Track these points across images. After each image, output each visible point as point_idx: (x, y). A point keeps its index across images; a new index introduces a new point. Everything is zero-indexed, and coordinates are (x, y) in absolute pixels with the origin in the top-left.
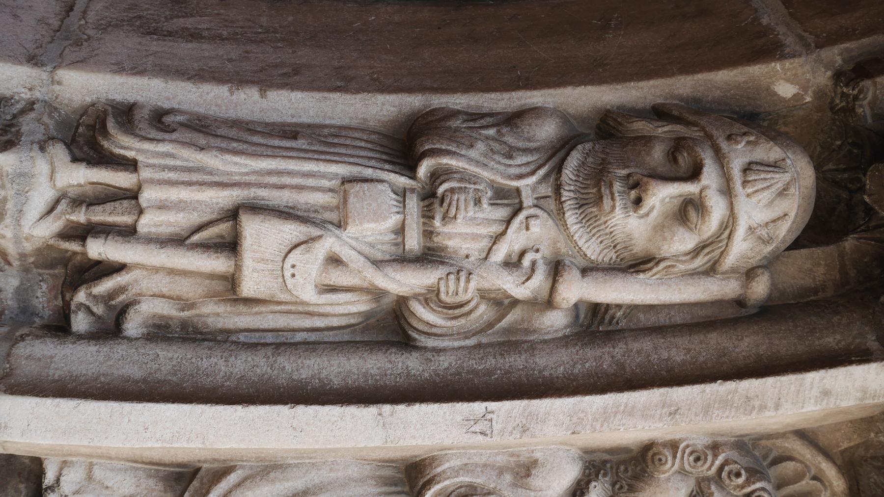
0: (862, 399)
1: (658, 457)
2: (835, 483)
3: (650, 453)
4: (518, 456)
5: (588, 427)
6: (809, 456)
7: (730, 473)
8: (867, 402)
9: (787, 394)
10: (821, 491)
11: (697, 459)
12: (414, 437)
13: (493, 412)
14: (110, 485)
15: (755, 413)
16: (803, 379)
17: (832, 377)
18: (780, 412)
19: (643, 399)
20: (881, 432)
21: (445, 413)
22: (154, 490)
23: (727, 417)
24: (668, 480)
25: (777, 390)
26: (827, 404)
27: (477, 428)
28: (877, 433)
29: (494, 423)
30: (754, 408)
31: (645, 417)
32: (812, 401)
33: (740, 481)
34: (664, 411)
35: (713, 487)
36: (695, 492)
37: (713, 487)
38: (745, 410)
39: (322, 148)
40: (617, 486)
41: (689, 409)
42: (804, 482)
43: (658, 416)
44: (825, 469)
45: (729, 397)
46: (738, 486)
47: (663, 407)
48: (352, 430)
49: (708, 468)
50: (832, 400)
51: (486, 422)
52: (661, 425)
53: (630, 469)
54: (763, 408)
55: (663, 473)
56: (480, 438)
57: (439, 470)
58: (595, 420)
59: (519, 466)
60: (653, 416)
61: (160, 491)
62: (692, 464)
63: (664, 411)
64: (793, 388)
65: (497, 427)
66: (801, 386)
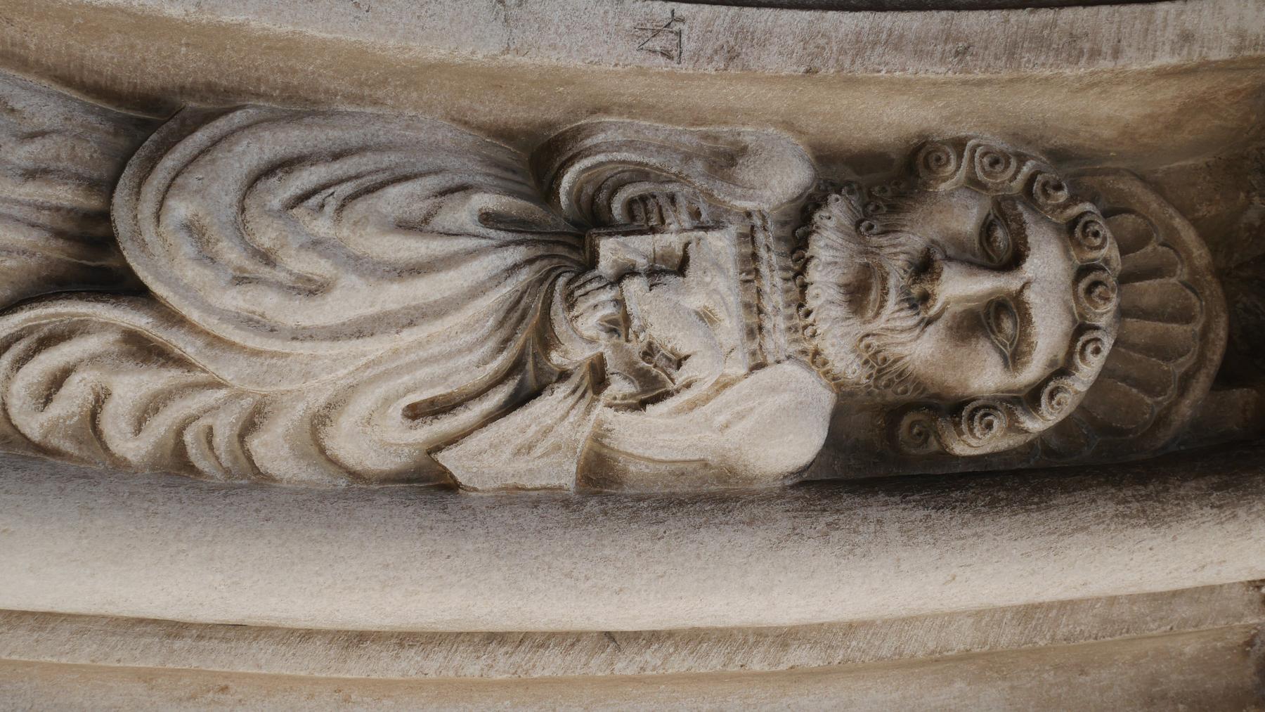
0: (1239, 49)
1: (934, 156)
2: (1196, 253)
3: (922, 155)
4: (716, 139)
5: (831, 62)
6: (1154, 206)
7: (1045, 185)
8: (1247, 53)
9: (1130, 34)
10: (1176, 264)
11: (994, 162)
12: (554, 47)
13: (682, 20)
14: (18, 106)
15: (1083, 61)
16: (1153, 12)
17: (1194, 11)
18: (1121, 62)
19: (916, 25)
20: (1255, 189)
21: (606, 12)
22: (98, 129)
23: (1043, 64)
24: (950, 194)
25: (1115, 26)
26: (1189, 54)
27: (657, 44)
28: (1248, 192)
29: (684, 38)
30: (1081, 53)
31: (919, 54)
32: (1167, 48)
33: (1062, 196)
34: (948, 48)
35: (1020, 208)
36: (992, 217)
37: (1020, 208)
38: (1070, 55)
39: (396, 295)
40: (871, 208)
41: (986, 48)
42: (1149, 248)
43: (938, 55)
44: (1180, 227)
45: (1046, 33)
46: (1059, 206)
47: (946, 41)
48: (452, 20)
49: (1013, 180)
50: (1196, 47)
51: (671, 36)
52: (943, 69)
53: (889, 189)
54: (1095, 54)
55: (944, 181)
56: (661, 60)
57: (589, 142)
58: (842, 51)
59: (716, 153)
60: (931, 54)
61: (108, 133)
62: (988, 168)
63: (948, 48)
64: (1138, 26)
65: (689, 46)
66: (1149, 22)
